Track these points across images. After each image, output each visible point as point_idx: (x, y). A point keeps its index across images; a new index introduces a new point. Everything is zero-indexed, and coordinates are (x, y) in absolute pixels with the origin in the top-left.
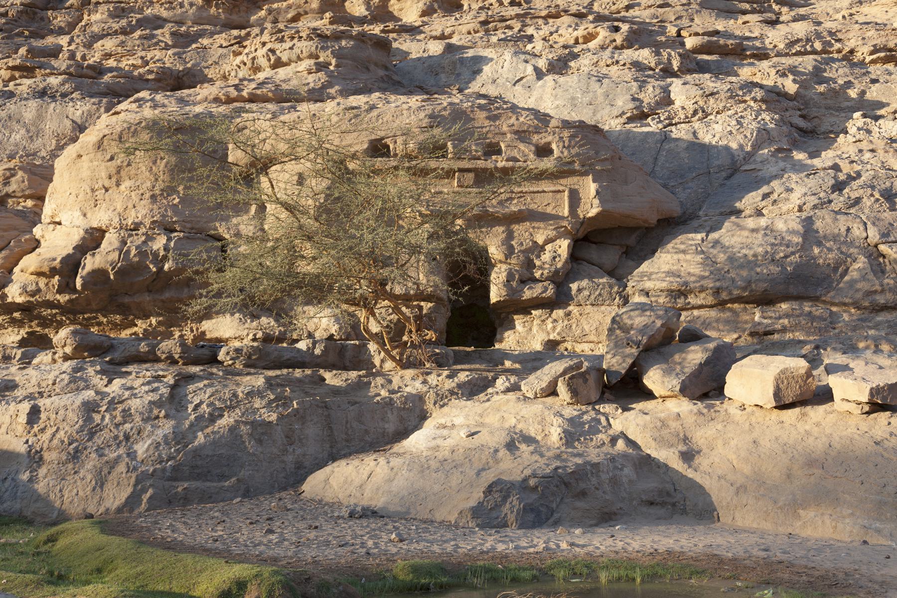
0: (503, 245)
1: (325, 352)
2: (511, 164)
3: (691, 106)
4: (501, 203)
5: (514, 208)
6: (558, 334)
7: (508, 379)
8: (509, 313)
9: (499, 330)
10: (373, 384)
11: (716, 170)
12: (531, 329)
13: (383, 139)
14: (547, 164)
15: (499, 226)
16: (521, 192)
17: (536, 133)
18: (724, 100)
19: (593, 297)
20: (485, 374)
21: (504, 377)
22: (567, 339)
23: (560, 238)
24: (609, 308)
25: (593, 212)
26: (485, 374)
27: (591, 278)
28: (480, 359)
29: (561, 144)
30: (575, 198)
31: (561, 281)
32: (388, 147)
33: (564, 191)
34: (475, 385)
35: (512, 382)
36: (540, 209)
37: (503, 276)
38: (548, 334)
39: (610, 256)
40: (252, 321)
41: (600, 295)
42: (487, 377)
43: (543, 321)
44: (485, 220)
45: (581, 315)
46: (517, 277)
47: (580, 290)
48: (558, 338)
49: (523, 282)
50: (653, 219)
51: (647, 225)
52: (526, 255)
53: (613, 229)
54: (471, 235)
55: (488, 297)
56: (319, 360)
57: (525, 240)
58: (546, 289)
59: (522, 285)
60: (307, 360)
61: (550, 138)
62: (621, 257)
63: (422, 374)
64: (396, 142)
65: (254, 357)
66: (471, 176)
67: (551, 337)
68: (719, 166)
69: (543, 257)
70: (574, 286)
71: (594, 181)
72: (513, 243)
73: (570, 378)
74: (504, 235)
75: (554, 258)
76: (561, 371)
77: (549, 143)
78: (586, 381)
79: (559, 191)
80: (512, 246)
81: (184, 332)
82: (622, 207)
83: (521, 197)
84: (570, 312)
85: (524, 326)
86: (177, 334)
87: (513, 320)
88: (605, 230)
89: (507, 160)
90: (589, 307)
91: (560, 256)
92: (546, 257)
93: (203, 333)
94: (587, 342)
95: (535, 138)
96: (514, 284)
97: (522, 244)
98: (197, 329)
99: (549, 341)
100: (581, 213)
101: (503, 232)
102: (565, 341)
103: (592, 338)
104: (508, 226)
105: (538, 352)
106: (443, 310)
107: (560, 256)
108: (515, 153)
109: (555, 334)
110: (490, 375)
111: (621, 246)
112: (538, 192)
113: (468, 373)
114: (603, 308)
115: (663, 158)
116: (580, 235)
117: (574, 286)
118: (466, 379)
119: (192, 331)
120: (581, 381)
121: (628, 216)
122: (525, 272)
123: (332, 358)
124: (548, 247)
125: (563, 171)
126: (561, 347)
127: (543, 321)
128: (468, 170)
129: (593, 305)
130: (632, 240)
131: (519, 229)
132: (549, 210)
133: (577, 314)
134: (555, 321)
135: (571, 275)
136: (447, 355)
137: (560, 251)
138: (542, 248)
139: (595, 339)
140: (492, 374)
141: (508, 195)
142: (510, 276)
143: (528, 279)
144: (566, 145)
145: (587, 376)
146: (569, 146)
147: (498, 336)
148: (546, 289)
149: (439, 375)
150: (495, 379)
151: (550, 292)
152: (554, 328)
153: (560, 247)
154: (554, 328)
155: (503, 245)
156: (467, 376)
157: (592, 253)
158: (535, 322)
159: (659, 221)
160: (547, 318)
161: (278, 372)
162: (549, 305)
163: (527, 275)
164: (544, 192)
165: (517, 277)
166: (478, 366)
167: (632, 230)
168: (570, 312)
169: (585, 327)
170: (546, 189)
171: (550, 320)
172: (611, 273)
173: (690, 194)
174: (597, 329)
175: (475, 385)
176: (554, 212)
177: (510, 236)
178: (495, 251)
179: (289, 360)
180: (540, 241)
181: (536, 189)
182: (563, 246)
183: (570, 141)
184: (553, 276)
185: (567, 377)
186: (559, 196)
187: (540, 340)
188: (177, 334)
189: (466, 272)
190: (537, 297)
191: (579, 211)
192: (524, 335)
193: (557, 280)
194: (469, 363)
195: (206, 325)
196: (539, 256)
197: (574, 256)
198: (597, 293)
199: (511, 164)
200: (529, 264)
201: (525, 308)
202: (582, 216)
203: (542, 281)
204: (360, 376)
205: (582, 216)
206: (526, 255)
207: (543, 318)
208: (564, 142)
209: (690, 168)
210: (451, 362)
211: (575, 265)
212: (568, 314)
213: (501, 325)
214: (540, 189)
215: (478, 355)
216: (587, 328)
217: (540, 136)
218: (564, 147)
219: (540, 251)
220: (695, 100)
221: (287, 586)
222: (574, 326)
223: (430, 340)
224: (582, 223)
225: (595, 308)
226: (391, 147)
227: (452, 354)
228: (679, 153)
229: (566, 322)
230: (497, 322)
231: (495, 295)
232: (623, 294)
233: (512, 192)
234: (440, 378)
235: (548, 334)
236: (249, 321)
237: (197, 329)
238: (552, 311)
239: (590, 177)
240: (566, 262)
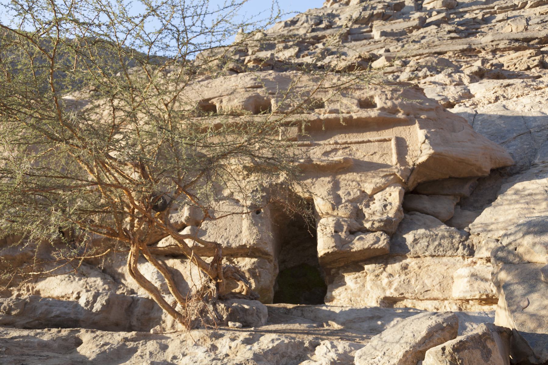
0: (329, 194)
1: (107, 307)
2: (334, 115)
3: (492, 95)
4: (326, 154)
5: (338, 157)
6: (396, 290)
7: (333, 346)
8: (339, 269)
9: (329, 287)
10: (139, 352)
11: (537, 129)
12: (364, 286)
13: (210, 99)
14: (373, 113)
15: (325, 176)
16: (346, 143)
17: (358, 89)
18: (520, 88)
19: (432, 247)
20: (299, 338)
21: (327, 343)
22: (406, 295)
23: (389, 186)
24: (452, 259)
25: (423, 158)
26: (299, 338)
27: (427, 227)
28: (302, 317)
29: (384, 97)
30: (402, 146)
31: (394, 229)
32: (215, 106)
33: (390, 140)
34: (283, 356)
35: (341, 351)
36: (366, 159)
37: (331, 229)
38: (384, 290)
39: (446, 205)
40: (80, 280)
41: (440, 245)
42: (302, 343)
43: (377, 276)
44: (310, 170)
45: (420, 268)
46: (345, 228)
47: (416, 241)
48: (396, 295)
49: (352, 233)
50: (487, 167)
51: (480, 174)
52: (355, 204)
53: (444, 180)
54: (298, 189)
55: (316, 252)
56: (97, 318)
57: (352, 190)
58: (378, 240)
59: (352, 236)
60: (81, 317)
61: (372, 93)
62: (455, 208)
63: (211, 337)
64: (221, 102)
65: (13, 313)
66: (295, 129)
67: (388, 294)
68: (538, 126)
69: (372, 206)
70: (409, 237)
71: (421, 128)
72: (340, 193)
73: (457, 349)
74: (330, 185)
75: (385, 206)
76: (424, 333)
77: (372, 97)
78: (487, 354)
79: (385, 140)
80: (339, 196)
81: (22, 292)
82: (453, 151)
83: (346, 148)
84: (407, 265)
85: (356, 283)
86: (15, 293)
87: (343, 277)
88: (436, 181)
89: (331, 112)
90: (429, 258)
91: (391, 204)
92: (376, 206)
93: (38, 292)
94: (430, 299)
95: (357, 94)
96: (343, 235)
97: (349, 194)
98: (33, 288)
99: (386, 298)
100: (410, 160)
101: (329, 182)
102: (404, 298)
103: (436, 294)
104: (334, 177)
105: (376, 308)
106: (269, 266)
107: (391, 204)
108: (337, 106)
109: (392, 290)
110: (307, 340)
111: (455, 195)
112: (363, 142)
113: (274, 336)
114: (445, 259)
115: (479, 126)
116: (411, 185)
117: (409, 237)
118: (271, 346)
119: (28, 290)
120: (477, 354)
121: (461, 161)
122: (355, 222)
123: (115, 315)
124: (377, 196)
125: (386, 121)
126: (400, 305)
127: (377, 276)
128: (294, 124)
129: (433, 256)
130: (466, 190)
131: (345, 179)
132: (376, 159)
133: (416, 267)
134: (391, 275)
135: (404, 225)
136: (258, 311)
137: (390, 199)
138: (371, 198)
139: (440, 296)
140: (311, 338)
141: (333, 147)
142: (338, 228)
143: (358, 230)
144: (389, 97)
145: (489, 345)
146: (392, 99)
147: (328, 294)
148: (378, 240)
149: (233, 340)
150: (314, 345)
151: (383, 242)
152: (390, 283)
153: (390, 195)
154: (390, 283)
155: (329, 194)
156: (273, 341)
157: (425, 203)
158: (368, 278)
159: (492, 170)
160: (382, 273)
161: (25, 333)
162: (383, 257)
163: (356, 225)
164: (369, 141)
165: (345, 228)
166: (296, 326)
167: (464, 180)
168: (407, 265)
169: (426, 281)
170: (371, 139)
171: (385, 274)
172: (448, 223)
173: (516, 149)
174: (440, 284)
175: (283, 356)
176: (381, 161)
177: (336, 186)
178: (321, 205)
179: (58, 316)
180: (369, 192)
181: (360, 140)
182: (394, 196)
183: (392, 94)
184: (385, 225)
185: (449, 344)
186: (385, 144)
187: (375, 297)
188: (15, 293)
189: (291, 228)
190: (369, 249)
191: (408, 158)
192: (355, 292)
193: (390, 230)
194: (286, 322)
195: (40, 286)
196: (368, 206)
197: (407, 206)
198: (436, 243)
199: (334, 115)
200: (357, 215)
201: (356, 263)
202: (411, 163)
203: (373, 232)
204: (126, 339)
205: (411, 163)
206: (355, 204)
207: (377, 272)
208: (386, 95)
209: (509, 131)
210: (263, 320)
211: (408, 216)
212: (405, 268)
213: (331, 282)
214: (365, 139)
215: (299, 313)
216: (428, 282)
217: (362, 92)
218: (387, 99)
219: (369, 201)
220: (494, 91)
221: (332, 363)
222: (413, 281)
223: (240, 293)
224: (412, 170)
225: (436, 260)
226: (218, 106)
227: (266, 311)
228: (494, 121)
229: (403, 277)
230: (327, 279)
231: (324, 245)
232: (467, 243)
233: (336, 143)
234: (233, 344)
235: (384, 290)
236: (77, 279)
237: (33, 288)
238: (386, 266)
239: (417, 125)
240: (398, 210)
